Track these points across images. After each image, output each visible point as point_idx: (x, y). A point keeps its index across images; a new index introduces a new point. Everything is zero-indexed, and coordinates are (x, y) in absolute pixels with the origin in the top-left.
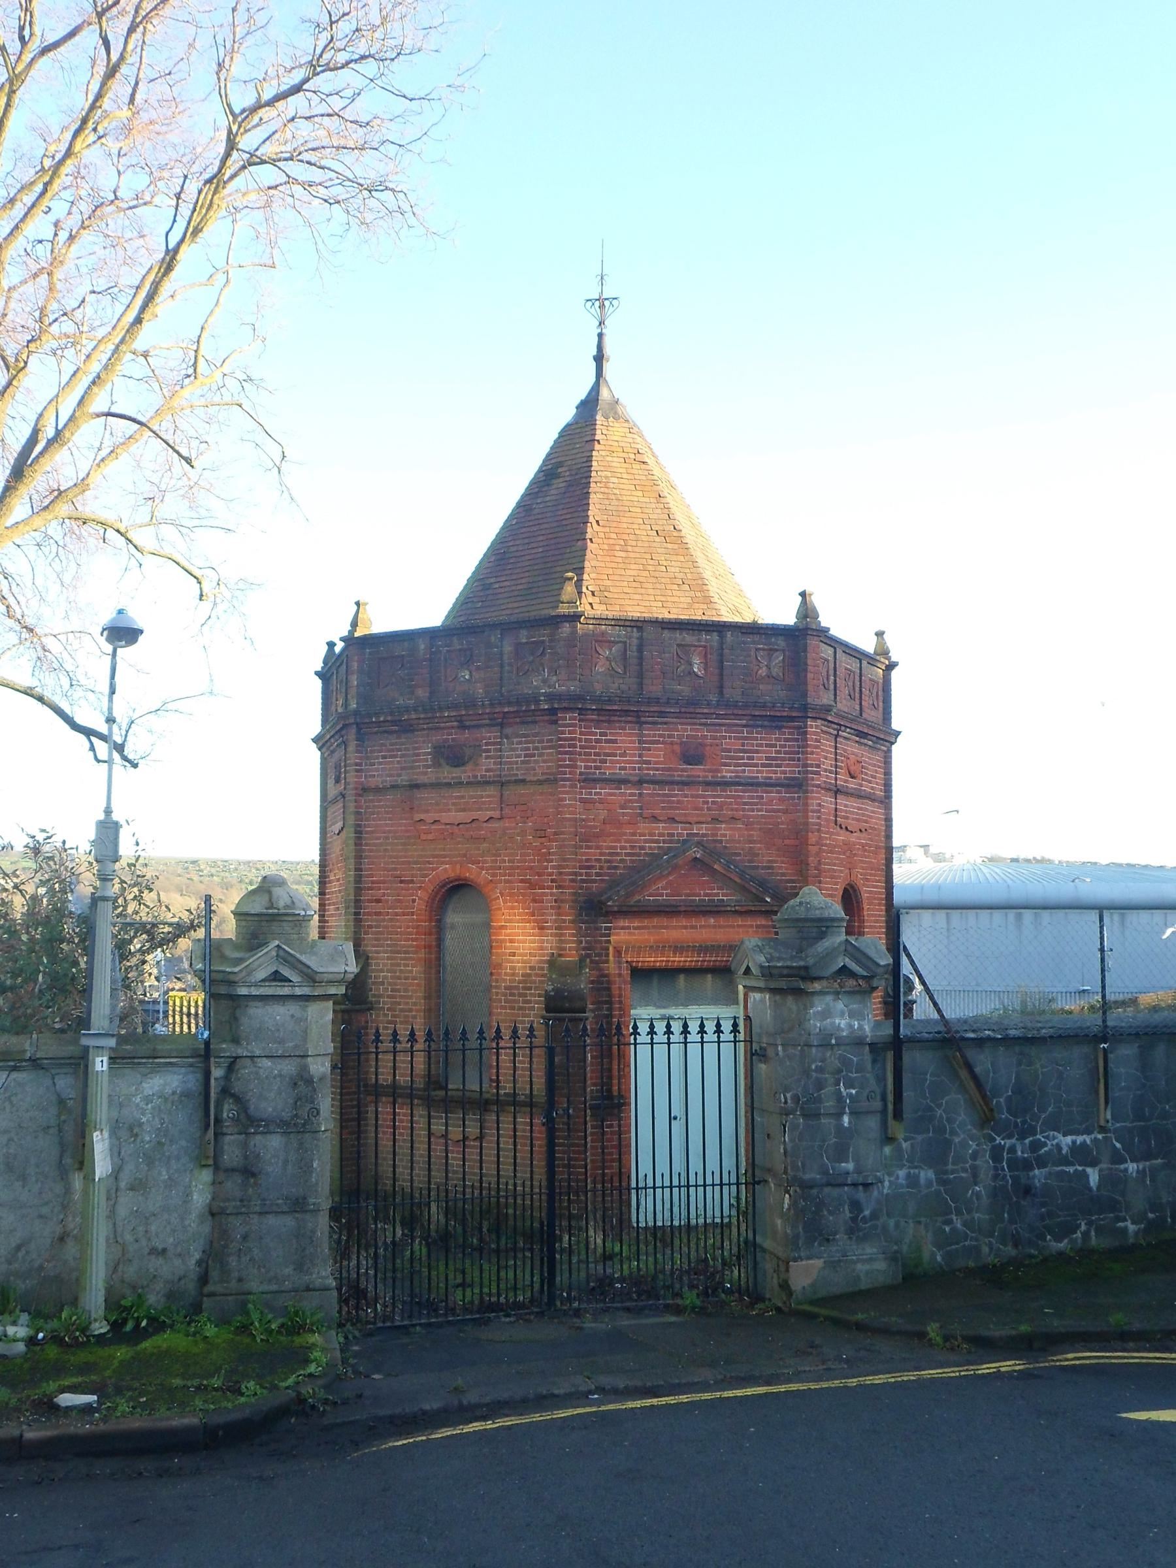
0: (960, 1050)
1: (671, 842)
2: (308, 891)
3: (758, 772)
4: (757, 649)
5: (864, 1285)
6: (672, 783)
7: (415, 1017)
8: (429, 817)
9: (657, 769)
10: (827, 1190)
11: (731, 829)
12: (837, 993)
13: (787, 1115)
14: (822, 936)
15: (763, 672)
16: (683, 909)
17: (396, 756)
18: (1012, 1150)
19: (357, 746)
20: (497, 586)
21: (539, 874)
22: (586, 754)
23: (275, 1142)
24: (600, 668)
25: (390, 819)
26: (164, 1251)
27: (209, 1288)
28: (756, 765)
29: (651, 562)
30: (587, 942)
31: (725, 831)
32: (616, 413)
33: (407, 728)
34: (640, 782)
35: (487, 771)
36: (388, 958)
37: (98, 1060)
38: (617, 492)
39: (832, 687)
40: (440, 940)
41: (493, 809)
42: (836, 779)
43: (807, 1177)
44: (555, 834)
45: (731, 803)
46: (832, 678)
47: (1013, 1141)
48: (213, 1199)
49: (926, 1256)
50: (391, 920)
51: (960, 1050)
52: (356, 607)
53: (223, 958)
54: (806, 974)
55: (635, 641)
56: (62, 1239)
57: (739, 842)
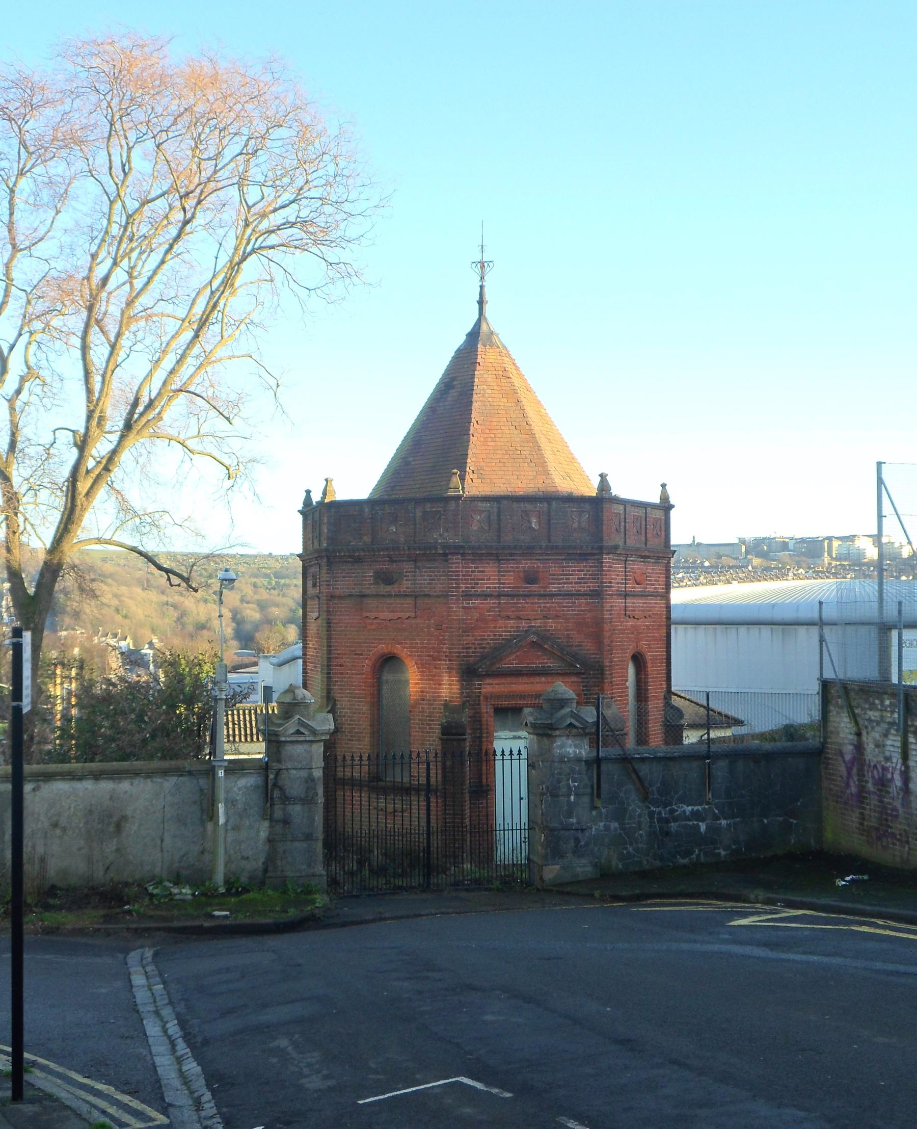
0: (631, 763)
1: (518, 631)
2: (266, 583)
3: (572, 587)
4: (572, 511)
5: (580, 878)
6: (518, 596)
7: (364, 737)
8: (372, 615)
9: (509, 588)
10: (562, 832)
11: (555, 623)
12: (568, 736)
13: (543, 795)
14: (562, 707)
15: (576, 525)
16: (525, 672)
17: (352, 577)
18: (660, 813)
19: (328, 570)
20: (413, 463)
21: (438, 652)
22: (465, 579)
23: (298, 808)
24: (474, 528)
25: (348, 615)
26: (248, 858)
27: (269, 874)
28: (571, 583)
29: (511, 448)
30: (467, 693)
31: (551, 624)
32: (491, 342)
33: (358, 560)
34: (499, 596)
35: (407, 588)
36: (349, 701)
37: (220, 771)
38: (490, 399)
39: (622, 530)
40: (379, 690)
41: (411, 611)
42: (625, 588)
43: (552, 825)
44: (447, 628)
45: (555, 607)
46: (623, 524)
47: (660, 809)
48: (270, 834)
49: (614, 863)
50: (349, 678)
51: (631, 763)
52: (325, 482)
53: (273, 723)
54: (551, 727)
55: (496, 510)
56: (202, 852)
57: (560, 630)
